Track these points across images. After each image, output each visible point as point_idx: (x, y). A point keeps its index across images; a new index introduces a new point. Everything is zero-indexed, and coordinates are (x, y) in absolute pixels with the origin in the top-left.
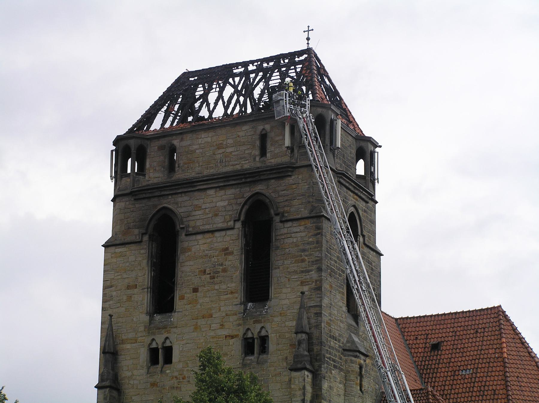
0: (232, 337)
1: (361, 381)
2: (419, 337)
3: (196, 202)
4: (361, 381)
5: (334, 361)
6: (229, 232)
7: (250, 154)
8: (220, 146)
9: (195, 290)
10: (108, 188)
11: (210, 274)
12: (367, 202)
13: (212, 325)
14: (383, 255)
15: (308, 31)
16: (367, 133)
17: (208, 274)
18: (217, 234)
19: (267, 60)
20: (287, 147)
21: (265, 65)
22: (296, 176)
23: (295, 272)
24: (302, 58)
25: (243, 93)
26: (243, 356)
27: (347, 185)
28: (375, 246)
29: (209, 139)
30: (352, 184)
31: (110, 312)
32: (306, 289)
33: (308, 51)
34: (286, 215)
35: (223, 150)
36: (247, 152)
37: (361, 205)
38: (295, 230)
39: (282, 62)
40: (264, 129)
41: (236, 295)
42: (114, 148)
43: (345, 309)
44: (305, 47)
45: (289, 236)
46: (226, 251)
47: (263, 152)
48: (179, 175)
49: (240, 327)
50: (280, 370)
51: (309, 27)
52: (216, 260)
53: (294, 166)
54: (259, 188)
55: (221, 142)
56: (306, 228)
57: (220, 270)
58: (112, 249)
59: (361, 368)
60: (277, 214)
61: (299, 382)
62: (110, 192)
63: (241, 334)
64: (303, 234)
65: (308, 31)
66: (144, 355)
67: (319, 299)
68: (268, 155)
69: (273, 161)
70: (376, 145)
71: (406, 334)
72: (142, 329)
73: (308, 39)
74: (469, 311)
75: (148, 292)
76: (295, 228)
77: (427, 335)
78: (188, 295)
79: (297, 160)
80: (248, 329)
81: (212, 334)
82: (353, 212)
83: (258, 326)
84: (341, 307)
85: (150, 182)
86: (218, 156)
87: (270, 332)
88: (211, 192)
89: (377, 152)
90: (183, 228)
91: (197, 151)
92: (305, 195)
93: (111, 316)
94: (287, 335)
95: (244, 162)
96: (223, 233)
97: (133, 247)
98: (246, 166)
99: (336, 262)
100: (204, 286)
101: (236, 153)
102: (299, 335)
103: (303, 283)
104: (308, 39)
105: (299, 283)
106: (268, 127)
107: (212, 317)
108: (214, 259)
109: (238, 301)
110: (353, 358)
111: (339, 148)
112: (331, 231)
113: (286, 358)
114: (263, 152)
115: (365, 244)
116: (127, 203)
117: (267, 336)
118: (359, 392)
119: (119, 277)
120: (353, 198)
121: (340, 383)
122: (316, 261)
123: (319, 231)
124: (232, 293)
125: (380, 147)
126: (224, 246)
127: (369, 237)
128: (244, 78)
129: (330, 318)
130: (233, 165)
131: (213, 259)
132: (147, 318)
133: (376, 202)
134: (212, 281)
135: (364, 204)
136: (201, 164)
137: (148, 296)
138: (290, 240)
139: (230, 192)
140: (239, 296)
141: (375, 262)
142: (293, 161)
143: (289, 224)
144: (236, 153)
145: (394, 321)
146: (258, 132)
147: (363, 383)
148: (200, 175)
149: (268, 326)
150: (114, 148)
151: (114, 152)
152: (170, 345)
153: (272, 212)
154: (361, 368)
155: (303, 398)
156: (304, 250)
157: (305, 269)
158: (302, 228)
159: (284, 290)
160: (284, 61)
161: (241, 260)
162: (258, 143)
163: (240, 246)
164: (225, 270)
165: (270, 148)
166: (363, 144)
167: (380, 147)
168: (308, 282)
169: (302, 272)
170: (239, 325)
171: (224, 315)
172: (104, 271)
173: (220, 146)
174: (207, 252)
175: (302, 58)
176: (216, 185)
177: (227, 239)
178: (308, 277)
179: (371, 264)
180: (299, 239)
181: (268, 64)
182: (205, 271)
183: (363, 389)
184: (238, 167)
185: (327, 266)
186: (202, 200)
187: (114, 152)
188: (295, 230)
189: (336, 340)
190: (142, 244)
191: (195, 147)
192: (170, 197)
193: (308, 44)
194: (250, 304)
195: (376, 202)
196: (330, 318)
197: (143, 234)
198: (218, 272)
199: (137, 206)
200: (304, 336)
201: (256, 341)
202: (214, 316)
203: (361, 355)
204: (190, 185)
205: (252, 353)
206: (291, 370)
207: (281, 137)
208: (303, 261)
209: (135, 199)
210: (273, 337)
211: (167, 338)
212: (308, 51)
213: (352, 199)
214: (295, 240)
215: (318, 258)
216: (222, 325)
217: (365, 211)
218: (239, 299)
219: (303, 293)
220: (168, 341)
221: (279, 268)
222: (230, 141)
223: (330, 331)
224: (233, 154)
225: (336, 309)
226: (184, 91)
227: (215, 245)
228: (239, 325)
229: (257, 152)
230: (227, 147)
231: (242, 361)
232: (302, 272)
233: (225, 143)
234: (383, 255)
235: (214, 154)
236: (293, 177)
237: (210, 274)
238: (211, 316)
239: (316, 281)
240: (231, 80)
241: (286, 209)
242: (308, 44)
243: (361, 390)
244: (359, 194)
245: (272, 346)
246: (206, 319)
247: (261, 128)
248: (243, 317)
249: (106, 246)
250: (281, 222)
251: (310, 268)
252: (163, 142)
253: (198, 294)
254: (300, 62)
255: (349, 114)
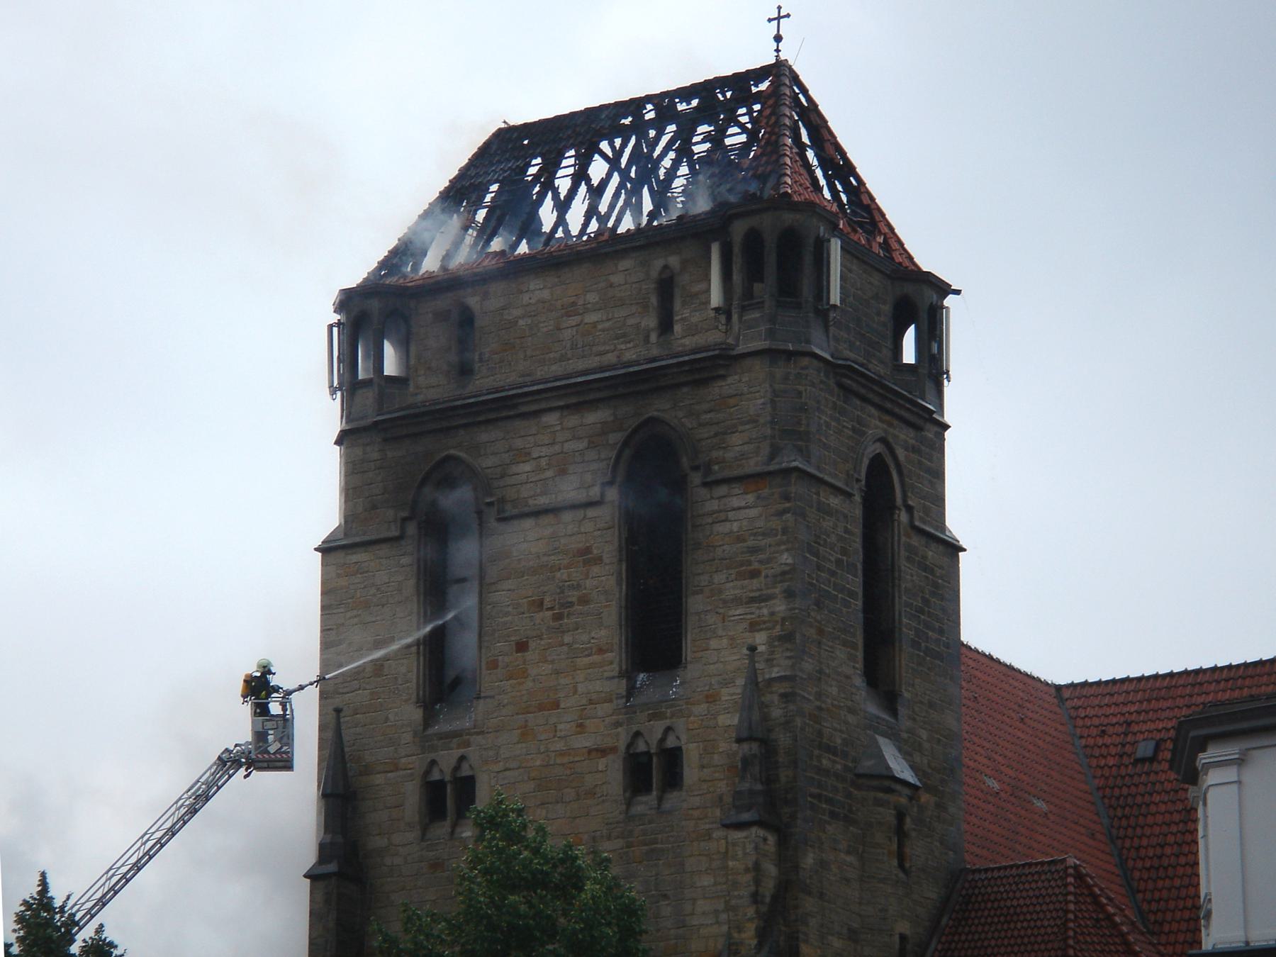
0: (603, 752)
1: (901, 846)
2: (1110, 730)
3: (519, 443)
4: (901, 846)
5: (829, 801)
6: (591, 513)
7: (638, 326)
8: (571, 310)
9: (522, 647)
10: (328, 415)
11: (552, 609)
12: (918, 428)
13: (560, 727)
14: (965, 550)
15: (779, 18)
16: (926, 261)
17: (548, 609)
18: (567, 516)
19: (686, 93)
20: (717, 310)
21: (681, 107)
22: (736, 377)
23: (737, 601)
24: (763, 86)
25: (633, 175)
26: (628, 795)
27: (863, 391)
28: (942, 526)
29: (546, 294)
30: (875, 388)
31: (337, 701)
32: (760, 639)
33: (779, 71)
34: (716, 467)
35: (576, 319)
36: (631, 321)
37: (904, 435)
38: (736, 502)
39: (720, 96)
40: (666, 267)
41: (609, 655)
42: (335, 318)
43: (859, 681)
44: (771, 60)
45: (722, 516)
46: (586, 556)
47: (666, 325)
48: (484, 382)
49: (620, 729)
50: (707, 826)
51: (779, 8)
52: (565, 577)
53: (735, 353)
54: (659, 407)
55: (573, 299)
56: (758, 498)
57: (574, 599)
58: (339, 557)
59: (901, 817)
60: (696, 468)
61: (745, 854)
62: (334, 425)
63: (622, 745)
64: (753, 513)
65: (779, 18)
66: (412, 796)
67: (789, 662)
68: (677, 328)
69: (687, 341)
70: (944, 289)
71: (1080, 722)
72: (407, 737)
73: (778, 38)
74: (1230, 667)
75: (418, 653)
76: (738, 498)
77: (1129, 724)
78: (507, 659)
79: (737, 339)
80: (638, 734)
81: (560, 746)
82: (879, 454)
83: (658, 727)
84: (848, 677)
85: (420, 398)
86: (567, 334)
87: (684, 738)
88: (551, 419)
89: (947, 308)
90: (490, 504)
91: (521, 322)
92: (756, 421)
93: (338, 711)
94: (723, 746)
95: (623, 347)
96: (580, 514)
97: (384, 550)
98: (630, 356)
99: (833, 574)
100: (540, 637)
101: (607, 325)
102: (746, 746)
103: (754, 627)
104: (778, 38)
105: (745, 625)
106: (674, 261)
107: (558, 706)
108: (562, 575)
109: (614, 669)
110: (881, 795)
111: (835, 306)
112: (819, 502)
113: (721, 798)
114: (666, 325)
115: (914, 527)
116: (368, 449)
117: (679, 749)
118: (901, 875)
119: (356, 620)
120: (881, 420)
121: (848, 853)
122: (784, 573)
123: (787, 505)
124: (601, 651)
125: (958, 292)
126: (580, 545)
127: (926, 511)
128: (634, 138)
129: (818, 703)
130: (601, 354)
131: (558, 575)
132: (417, 714)
133: (947, 427)
134: (556, 624)
135: (912, 433)
136: (529, 353)
137: (418, 660)
138: (720, 528)
139: (594, 418)
140: (615, 660)
141: (941, 568)
142: (730, 341)
143: (723, 490)
144: (607, 325)
145: (1053, 691)
146: (654, 274)
147: (907, 850)
148: (528, 379)
149: (680, 724)
150: (335, 318)
151: (335, 330)
152: (468, 773)
153: (685, 462)
154: (901, 817)
155: (753, 888)
156: (754, 550)
157: (757, 594)
158: (750, 498)
159: (714, 644)
160: (724, 96)
161: (620, 573)
162: (654, 300)
163: (616, 544)
164: (584, 600)
165: (682, 312)
166: (909, 289)
167: (958, 292)
168: (764, 622)
169: (752, 600)
170: (617, 724)
171: (584, 701)
172: (323, 608)
173: (571, 310)
174: (545, 559)
175: (763, 86)
176: (561, 403)
177: (588, 526)
178: (529, 684)
179: (932, 572)
180: (745, 523)
181: (689, 104)
182: (541, 603)
183: (907, 865)
184: (611, 358)
185: (812, 584)
186: (531, 439)
187: (335, 330)
188: (736, 502)
189: (835, 754)
190: (403, 543)
191: (516, 312)
192: (462, 432)
193: (778, 50)
194: (642, 675)
195: (947, 427)
196: (818, 703)
197: (404, 520)
198: (571, 604)
199: (390, 454)
200: (755, 747)
201: (655, 759)
202: (562, 706)
203: (898, 787)
204: (506, 408)
205: (648, 790)
206: (727, 826)
207: (702, 286)
208: (754, 574)
209: (385, 440)
210: (692, 754)
211: (462, 758)
212: (779, 71)
213: (876, 425)
214: (735, 526)
215: (787, 568)
216: (581, 725)
217: (915, 450)
218: (615, 666)
219: (752, 649)
220: (465, 766)
221: (701, 592)
222: (592, 297)
223: (820, 734)
224: (600, 327)
225: (834, 683)
226: (511, 164)
227: (563, 541)
228: (617, 724)
229: (651, 321)
230: (587, 311)
231: (624, 807)
232: (752, 600)
233: (580, 302)
234: (965, 550)
235: (559, 329)
236: (730, 380)
237: (552, 609)
238: (556, 705)
239: (784, 619)
240: (604, 146)
241: (715, 454)
242: (778, 50)
243: (901, 866)
244: (897, 410)
245: (690, 774)
246: (546, 713)
247: (658, 264)
248: (626, 707)
249: (327, 549)
250: (705, 484)
251: (769, 591)
252: (444, 302)
253: (529, 655)
254: (759, 97)
255: (878, 217)
